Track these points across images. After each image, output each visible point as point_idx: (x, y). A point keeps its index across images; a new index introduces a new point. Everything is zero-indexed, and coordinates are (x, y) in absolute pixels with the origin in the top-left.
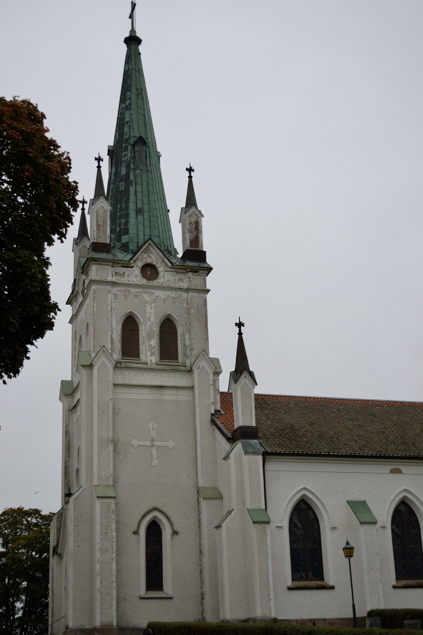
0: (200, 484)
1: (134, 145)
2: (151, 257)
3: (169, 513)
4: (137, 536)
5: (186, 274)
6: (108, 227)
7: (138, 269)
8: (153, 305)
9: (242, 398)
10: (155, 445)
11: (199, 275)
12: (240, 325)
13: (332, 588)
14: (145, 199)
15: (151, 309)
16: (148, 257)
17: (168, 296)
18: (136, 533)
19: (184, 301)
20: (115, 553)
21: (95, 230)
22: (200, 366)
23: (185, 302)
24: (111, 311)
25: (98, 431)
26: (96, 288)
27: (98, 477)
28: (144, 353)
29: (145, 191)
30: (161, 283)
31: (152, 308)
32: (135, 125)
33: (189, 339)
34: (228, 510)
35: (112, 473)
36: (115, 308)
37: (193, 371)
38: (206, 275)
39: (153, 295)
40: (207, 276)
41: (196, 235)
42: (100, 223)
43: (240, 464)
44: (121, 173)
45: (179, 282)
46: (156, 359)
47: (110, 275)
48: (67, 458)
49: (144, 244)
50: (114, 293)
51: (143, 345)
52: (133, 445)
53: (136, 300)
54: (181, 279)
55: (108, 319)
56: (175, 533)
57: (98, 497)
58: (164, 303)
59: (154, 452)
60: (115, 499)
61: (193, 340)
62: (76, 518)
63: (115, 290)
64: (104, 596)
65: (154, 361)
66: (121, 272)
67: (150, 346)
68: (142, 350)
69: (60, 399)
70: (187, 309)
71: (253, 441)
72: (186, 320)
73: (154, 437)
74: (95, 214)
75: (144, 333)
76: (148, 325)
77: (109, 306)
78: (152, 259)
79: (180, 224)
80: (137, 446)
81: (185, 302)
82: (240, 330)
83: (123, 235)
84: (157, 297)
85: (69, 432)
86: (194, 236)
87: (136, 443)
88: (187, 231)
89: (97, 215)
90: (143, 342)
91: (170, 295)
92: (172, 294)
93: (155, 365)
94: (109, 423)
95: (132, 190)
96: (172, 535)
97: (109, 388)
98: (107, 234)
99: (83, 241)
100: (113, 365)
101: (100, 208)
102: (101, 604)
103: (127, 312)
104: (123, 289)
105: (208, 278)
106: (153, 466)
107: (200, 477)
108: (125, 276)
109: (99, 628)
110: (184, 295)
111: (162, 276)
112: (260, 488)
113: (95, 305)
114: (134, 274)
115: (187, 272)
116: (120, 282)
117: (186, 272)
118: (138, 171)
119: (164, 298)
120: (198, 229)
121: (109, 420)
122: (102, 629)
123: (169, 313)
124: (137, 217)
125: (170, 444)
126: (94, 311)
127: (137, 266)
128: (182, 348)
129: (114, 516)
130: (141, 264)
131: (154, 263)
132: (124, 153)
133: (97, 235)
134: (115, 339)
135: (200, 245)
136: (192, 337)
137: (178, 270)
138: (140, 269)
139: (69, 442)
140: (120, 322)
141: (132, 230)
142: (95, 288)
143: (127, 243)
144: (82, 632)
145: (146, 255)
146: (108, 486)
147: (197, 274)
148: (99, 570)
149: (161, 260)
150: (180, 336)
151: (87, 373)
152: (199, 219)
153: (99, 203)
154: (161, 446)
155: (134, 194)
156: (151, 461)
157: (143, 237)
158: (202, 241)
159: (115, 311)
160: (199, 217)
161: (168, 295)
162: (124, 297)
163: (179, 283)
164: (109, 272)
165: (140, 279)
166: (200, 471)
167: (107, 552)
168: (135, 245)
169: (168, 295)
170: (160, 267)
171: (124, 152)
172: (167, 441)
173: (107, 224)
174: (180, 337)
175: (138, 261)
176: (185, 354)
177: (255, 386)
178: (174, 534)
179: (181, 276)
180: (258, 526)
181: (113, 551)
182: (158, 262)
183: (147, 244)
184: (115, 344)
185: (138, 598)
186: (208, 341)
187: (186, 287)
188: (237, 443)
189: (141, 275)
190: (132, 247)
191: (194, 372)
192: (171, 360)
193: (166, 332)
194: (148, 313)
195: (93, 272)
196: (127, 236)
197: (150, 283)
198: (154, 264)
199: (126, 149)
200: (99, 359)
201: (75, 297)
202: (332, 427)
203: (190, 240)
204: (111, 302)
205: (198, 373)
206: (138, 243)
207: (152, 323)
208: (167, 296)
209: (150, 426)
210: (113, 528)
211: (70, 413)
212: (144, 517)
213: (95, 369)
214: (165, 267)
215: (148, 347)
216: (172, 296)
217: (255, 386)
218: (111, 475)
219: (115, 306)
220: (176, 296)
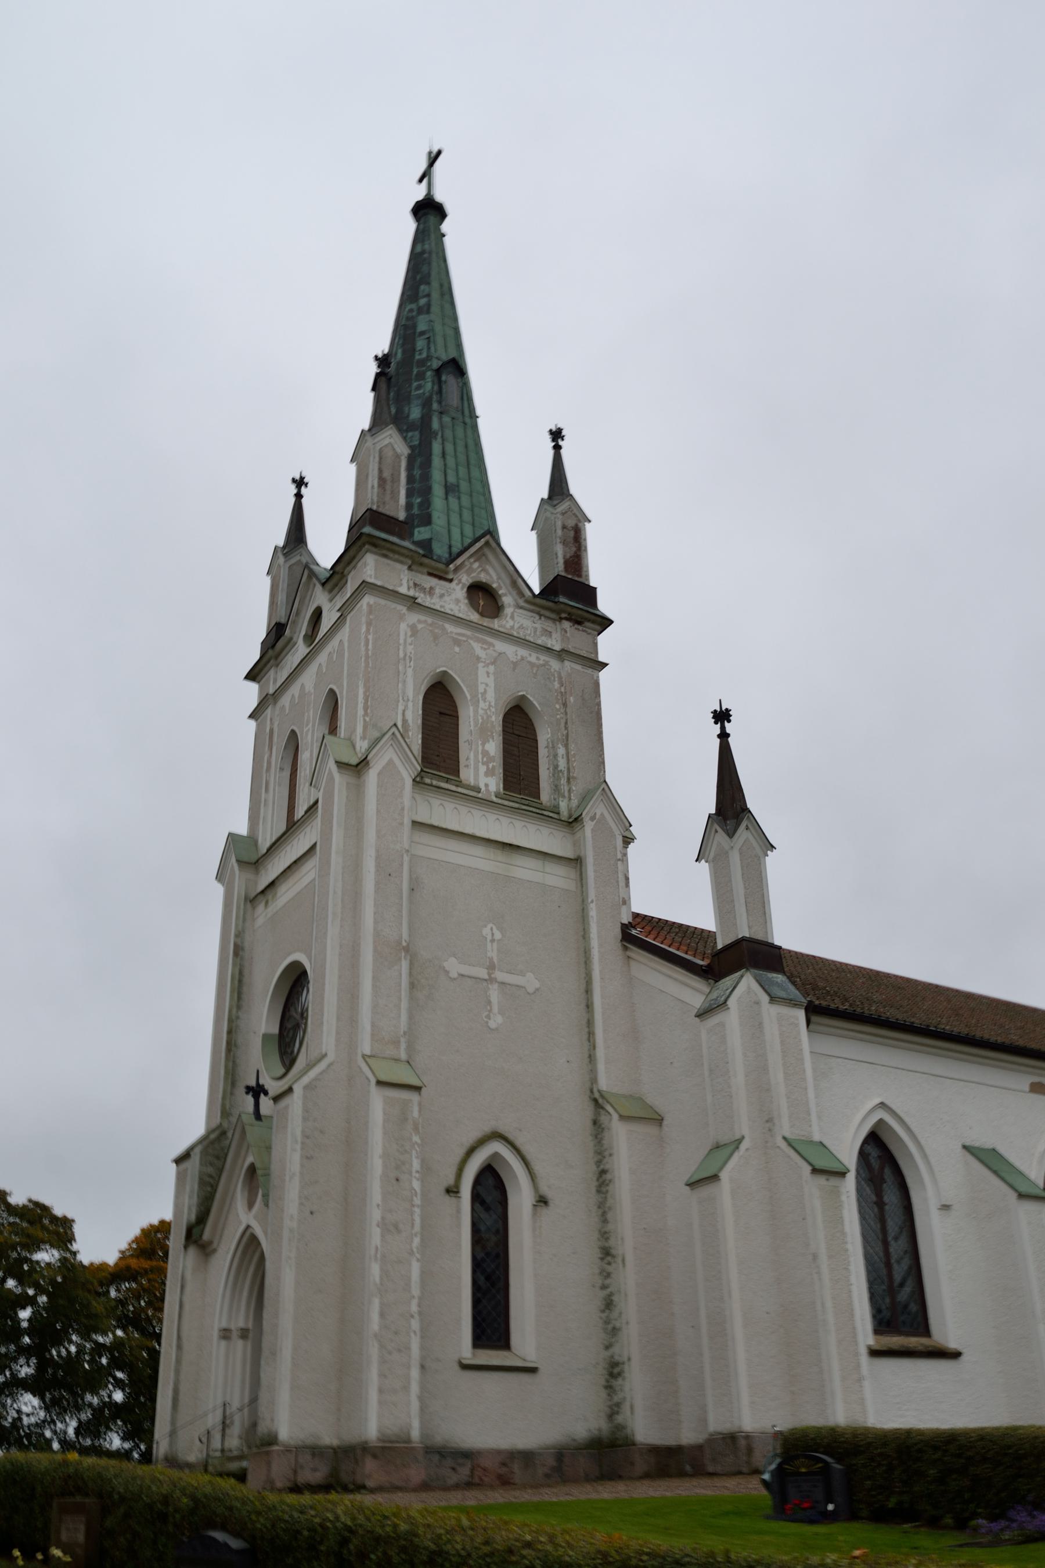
0: (604, 1083)
1: (438, 372)
2: (487, 573)
3: (528, 1149)
4: (454, 1200)
5: (558, 623)
6: (401, 488)
7: (462, 589)
8: (492, 668)
9: (743, 874)
10: (496, 979)
11: (583, 631)
12: (722, 716)
13: (956, 1355)
14: (462, 471)
15: (488, 676)
16: (482, 570)
17: (522, 659)
18: (452, 1191)
19: (554, 675)
20: (419, 1236)
21: (376, 485)
22: (595, 814)
23: (556, 679)
24: (404, 659)
25: (376, 922)
26: (375, 603)
27: (372, 1035)
28: (472, 766)
29: (462, 458)
30: (507, 629)
31: (490, 675)
32: (440, 340)
33: (565, 756)
34: (717, 1143)
35: (406, 1030)
36: (412, 656)
37: (583, 823)
38: (596, 633)
39: (491, 648)
40: (599, 634)
41: (575, 553)
42: (386, 474)
43: (755, 1027)
44: (408, 416)
45: (542, 635)
46: (497, 785)
47: (405, 582)
48: (234, 1010)
49: (477, 540)
50: (410, 624)
51: (471, 750)
52: (447, 972)
53: (457, 649)
54: (546, 630)
55: (399, 675)
56: (542, 1201)
57: (379, 1083)
58: (514, 669)
59: (494, 994)
60: (420, 1094)
61: (575, 761)
62: (308, 1137)
63: (413, 618)
64: (390, 1353)
65: (493, 788)
66: (425, 586)
67: (485, 753)
68: (468, 759)
69: (220, 876)
70: (560, 695)
71: (775, 975)
72: (558, 716)
73: (495, 960)
74: (377, 455)
75: (472, 723)
76: (482, 709)
77: (401, 647)
78: (491, 576)
79: (534, 532)
80: (455, 975)
81: (556, 679)
82: (723, 728)
83: (418, 526)
84: (500, 654)
85: (243, 949)
86: (572, 553)
87: (454, 967)
88: (558, 540)
89: (381, 458)
90: (470, 743)
91: (527, 658)
92: (530, 655)
93: (496, 797)
94: (402, 905)
95: (436, 448)
96: (534, 1205)
97: (402, 824)
98: (398, 502)
99: (299, 551)
100: (413, 772)
101: (386, 446)
102: (382, 1375)
103: (438, 671)
104: (430, 620)
105: (601, 638)
106: (493, 1030)
107: (601, 1067)
108: (435, 596)
109: (376, 1447)
110: (555, 664)
111: (509, 615)
112: (806, 1089)
113: (370, 637)
114: (453, 596)
115: (561, 619)
116: (423, 604)
117: (558, 618)
118: (446, 419)
119: (515, 660)
120: (579, 542)
121: (401, 898)
122: (383, 1448)
123: (524, 693)
124: (447, 499)
125: (530, 981)
126: (367, 650)
127: (460, 581)
128: (550, 773)
129: (418, 1137)
130: (467, 580)
131: (494, 586)
132: (415, 384)
133: (378, 496)
134: (410, 722)
135: (584, 574)
136: (572, 753)
137: (543, 612)
138: (465, 589)
139: (241, 973)
140: (421, 687)
141: (438, 518)
142: (372, 602)
143: (430, 540)
144: (313, 1455)
145: (476, 565)
146: (397, 1060)
147: (581, 628)
148: (378, 1280)
149: (508, 582)
150: (547, 747)
151: (348, 783)
152: (580, 525)
153: (386, 437)
154: (509, 984)
155: (441, 455)
156: (488, 1017)
157: (460, 539)
158: (587, 567)
159: (412, 662)
160: (579, 521)
161: (522, 656)
162: (432, 639)
163: (543, 638)
164: (402, 576)
165: (466, 609)
166: (600, 1053)
167: (399, 1231)
168: (446, 548)
169: (522, 656)
170: (505, 595)
171: (416, 381)
172: (522, 974)
173: (399, 480)
174: (546, 750)
175: (461, 572)
176: (556, 786)
177: (769, 852)
178: (539, 1204)
179: (547, 624)
180: (821, 1180)
181: (413, 1232)
182: (502, 585)
183: (482, 540)
184: (410, 734)
185: (457, 1368)
186: (604, 768)
187: (557, 647)
188: (742, 976)
189: (466, 601)
190: (439, 550)
191: (584, 826)
192: (524, 795)
193: (514, 734)
194: (482, 683)
195: (368, 568)
196: (428, 528)
197: (486, 622)
198: (491, 587)
199: (421, 376)
200: (383, 751)
201: (277, 657)
202: (865, 991)
203: (564, 558)
204: (405, 641)
205: (592, 830)
206: (450, 547)
207: (490, 706)
208: (519, 658)
209: (487, 931)
210: (414, 1170)
211: (249, 905)
212: (471, 1151)
213: (372, 776)
214: (517, 597)
215: (480, 756)
216: (529, 659)
217: (769, 852)
218: (402, 1033)
219: (413, 652)
220: (537, 662)
